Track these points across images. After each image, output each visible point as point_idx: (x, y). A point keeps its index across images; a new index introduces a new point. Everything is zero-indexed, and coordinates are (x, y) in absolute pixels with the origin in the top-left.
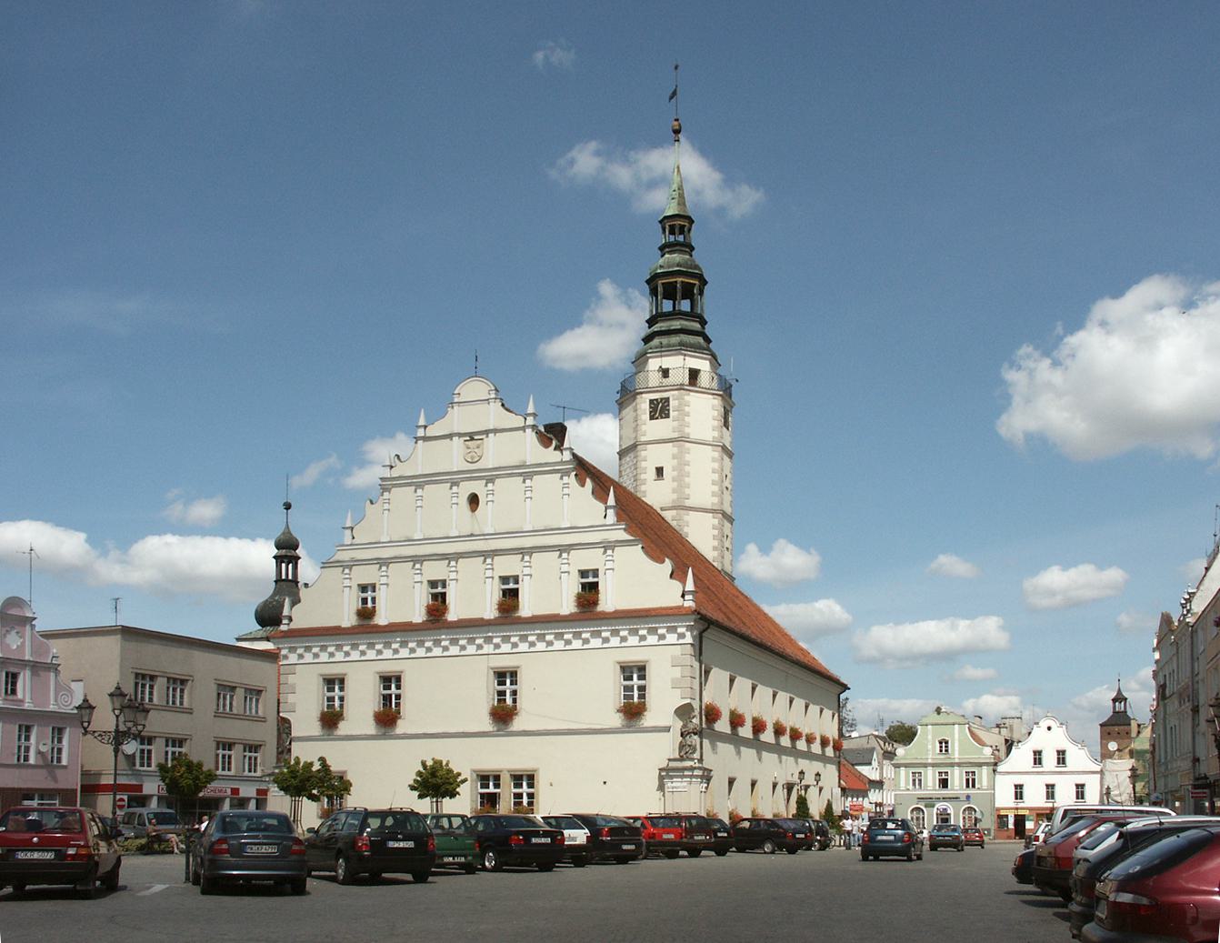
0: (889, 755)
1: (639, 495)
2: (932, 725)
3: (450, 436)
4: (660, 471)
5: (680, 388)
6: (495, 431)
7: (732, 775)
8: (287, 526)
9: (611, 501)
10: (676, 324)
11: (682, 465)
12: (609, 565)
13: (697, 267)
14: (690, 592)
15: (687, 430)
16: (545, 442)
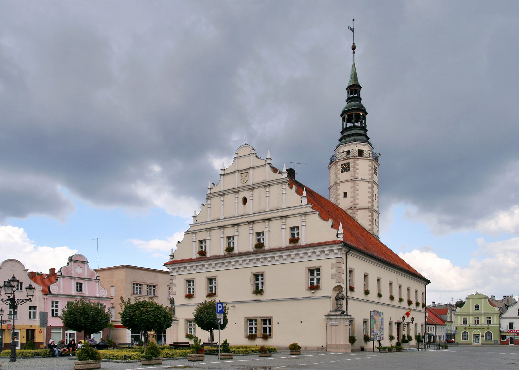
2: (472, 299)
4: (345, 194)
5: (354, 158)
6: (253, 168)
9: (304, 194)
11: (355, 190)
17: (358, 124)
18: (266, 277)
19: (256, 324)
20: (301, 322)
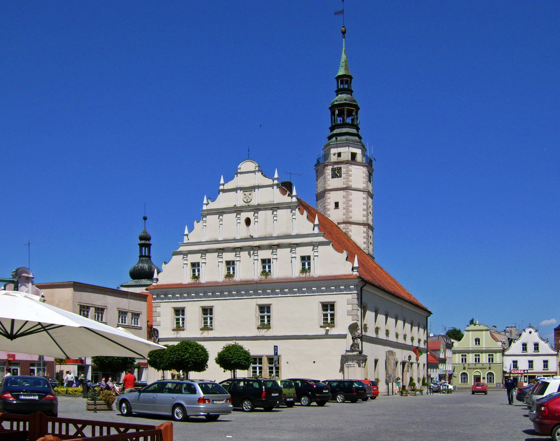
0: (449, 346)
1: (327, 216)
3: (235, 190)
4: (337, 205)
5: (347, 162)
6: (259, 187)
7: (376, 358)
8: (145, 229)
9: (317, 222)
10: (345, 130)
12: (316, 254)
13: (354, 101)
14: (356, 268)
15: (350, 183)
16: (284, 193)
17: (349, 120)
18: (273, 309)
19: (261, 363)
20: (314, 362)
